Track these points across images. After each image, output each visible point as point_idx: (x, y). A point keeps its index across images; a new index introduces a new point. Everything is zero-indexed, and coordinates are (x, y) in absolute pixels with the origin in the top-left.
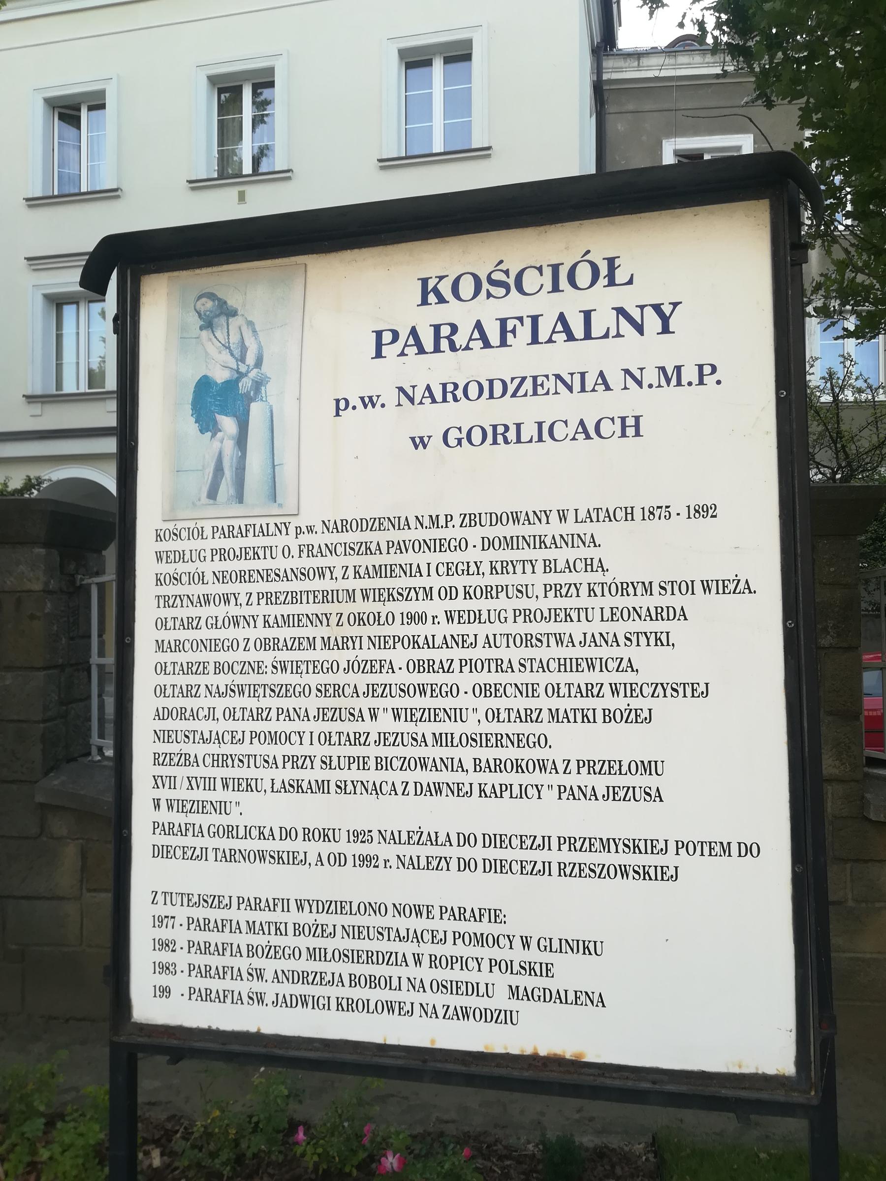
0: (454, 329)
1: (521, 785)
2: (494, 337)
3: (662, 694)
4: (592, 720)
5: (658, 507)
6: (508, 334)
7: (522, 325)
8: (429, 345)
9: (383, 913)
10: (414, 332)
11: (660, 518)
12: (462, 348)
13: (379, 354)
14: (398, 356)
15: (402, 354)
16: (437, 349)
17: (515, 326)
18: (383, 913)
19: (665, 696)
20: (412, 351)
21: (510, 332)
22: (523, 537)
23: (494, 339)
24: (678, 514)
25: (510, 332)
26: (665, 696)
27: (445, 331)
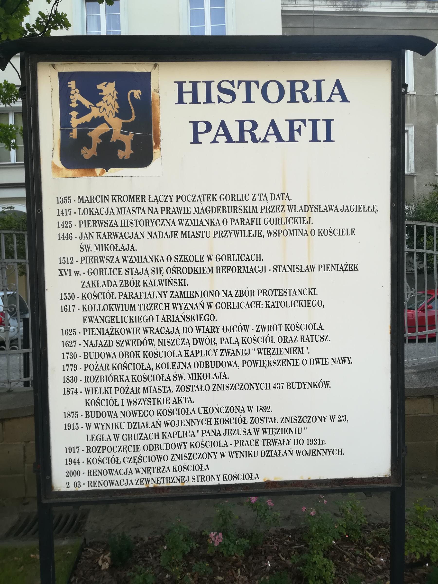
0: (255, 125)
1: (238, 302)
2: (285, 134)
3: (143, 404)
4: (109, 393)
5: (72, 412)
6: (295, 132)
7: (306, 126)
8: (235, 136)
9: (217, 295)
10: (223, 124)
11: (73, 417)
12: (261, 140)
13: (196, 141)
14: (211, 143)
15: (215, 141)
16: (242, 140)
17: (300, 126)
18: (217, 295)
19: (145, 404)
20: (222, 139)
21: (297, 130)
22: (299, 230)
23: (285, 135)
24: (82, 427)
25: (297, 130)
26: (145, 404)
27: (248, 126)
